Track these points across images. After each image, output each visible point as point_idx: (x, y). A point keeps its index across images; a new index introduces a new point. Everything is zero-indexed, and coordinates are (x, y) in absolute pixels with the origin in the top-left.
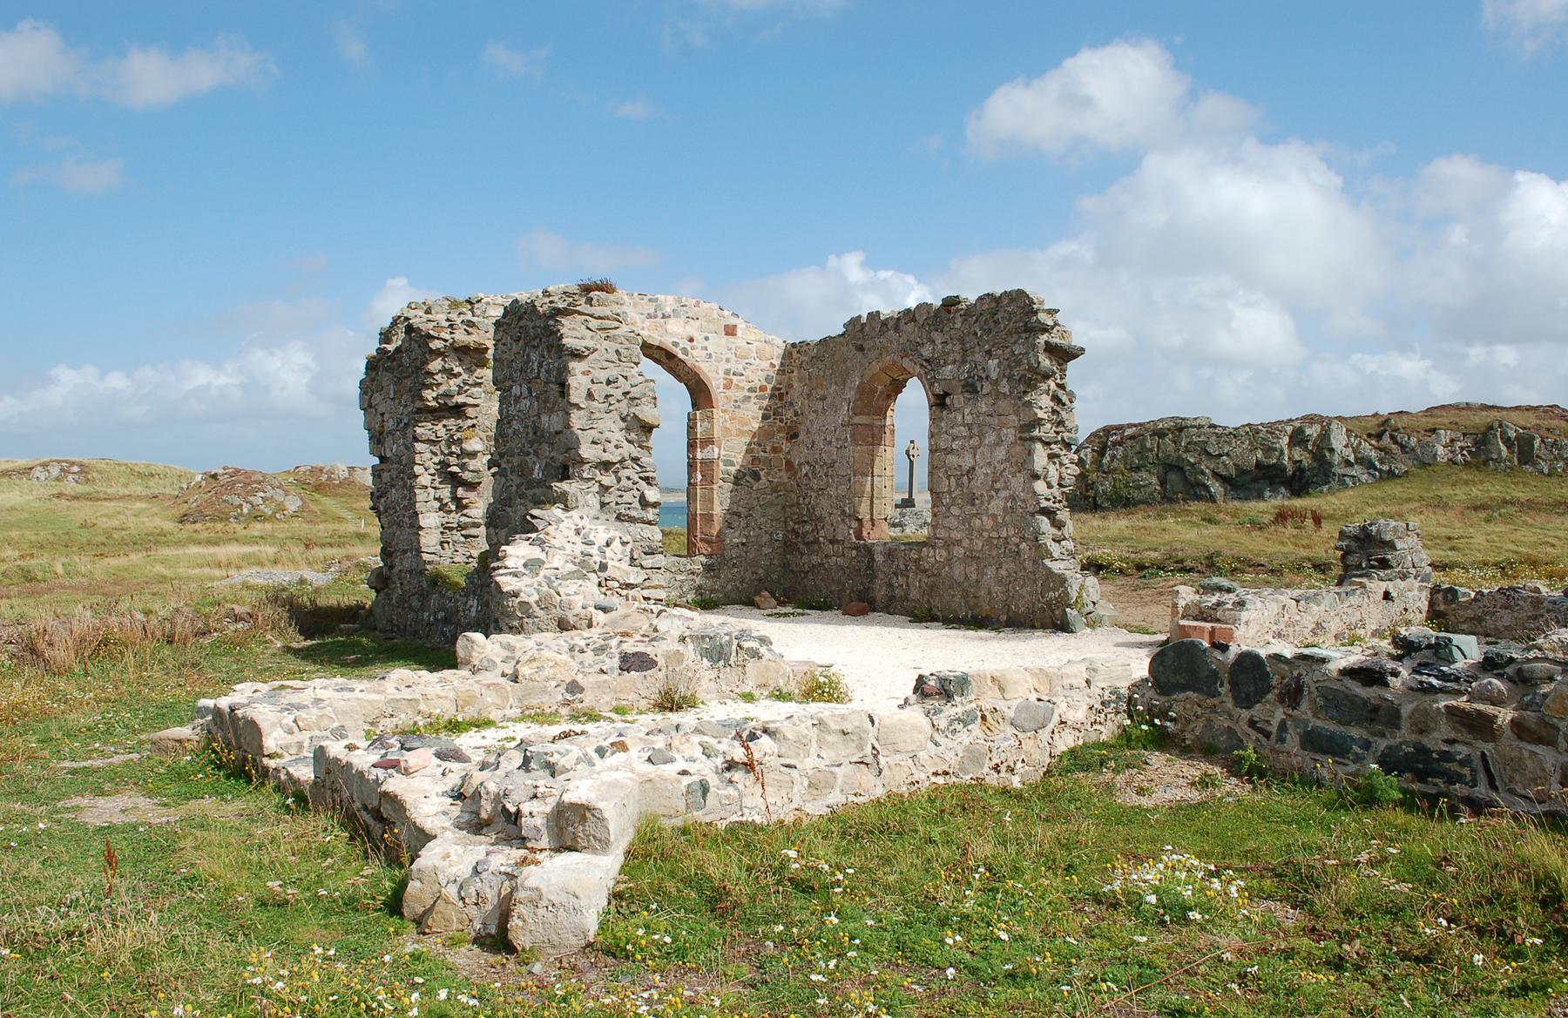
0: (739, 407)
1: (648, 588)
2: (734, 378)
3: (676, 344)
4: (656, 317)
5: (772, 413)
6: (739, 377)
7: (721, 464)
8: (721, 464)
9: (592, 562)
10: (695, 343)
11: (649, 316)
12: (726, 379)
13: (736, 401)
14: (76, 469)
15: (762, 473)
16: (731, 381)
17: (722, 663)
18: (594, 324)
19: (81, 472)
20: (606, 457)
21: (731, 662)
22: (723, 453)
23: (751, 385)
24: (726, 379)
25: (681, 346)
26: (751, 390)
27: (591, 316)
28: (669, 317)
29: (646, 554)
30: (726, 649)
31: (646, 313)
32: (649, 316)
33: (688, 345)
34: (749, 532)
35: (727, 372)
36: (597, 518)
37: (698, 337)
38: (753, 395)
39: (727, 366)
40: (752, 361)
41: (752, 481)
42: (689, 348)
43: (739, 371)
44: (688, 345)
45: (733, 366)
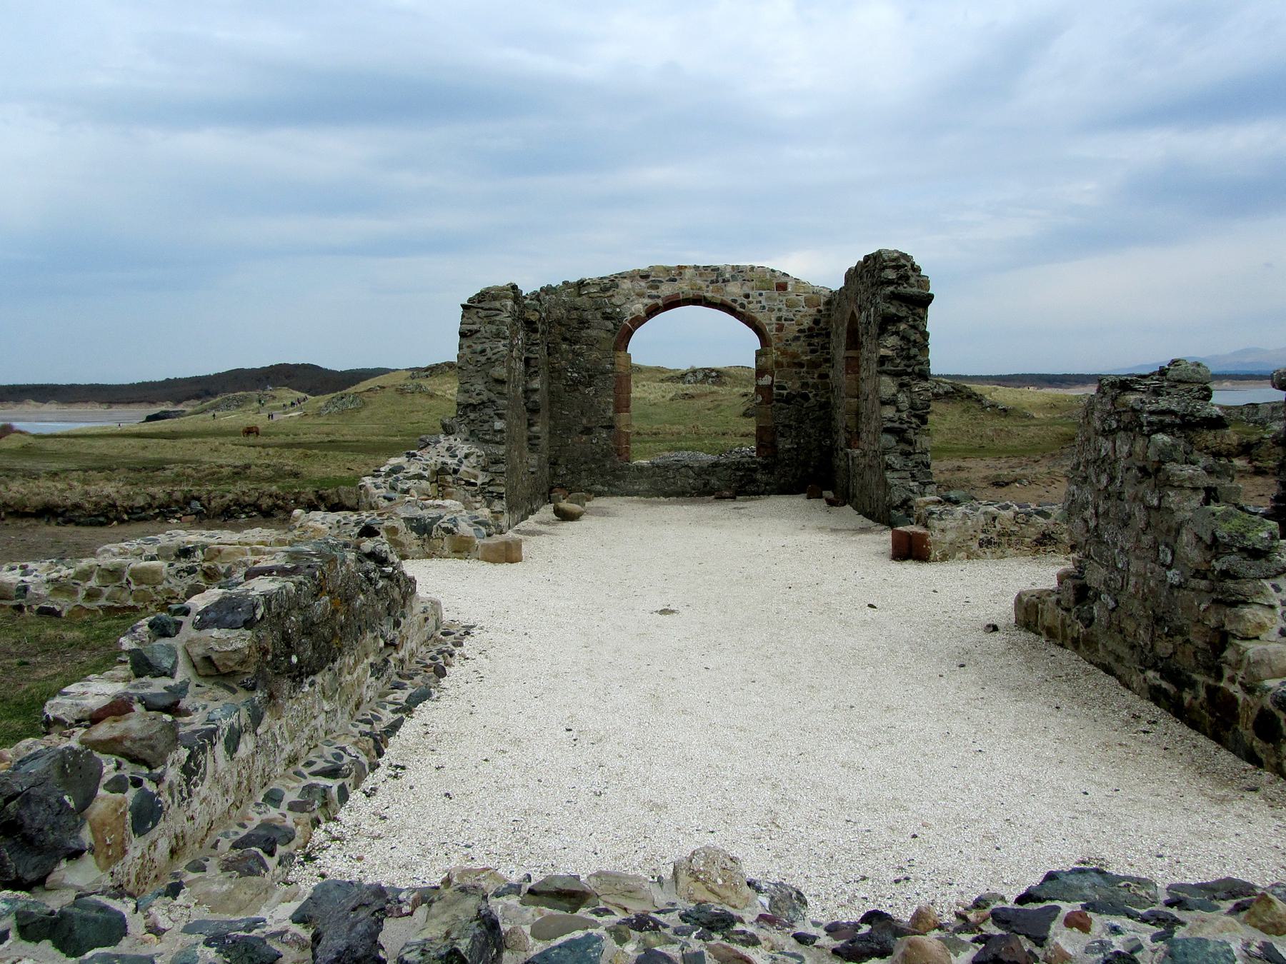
0: (790, 345)
1: (492, 485)
2: (786, 323)
3: (734, 301)
4: (717, 282)
5: (819, 348)
6: (789, 322)
7: (774, 389)
8: (774, 389)
9: (448, 468)
10: (751, 299)
11: (712, 282)
12: (778, 324)
13: (787, 341)
14: (714, 374)
15: (811, 395)
16: (783, 325)
17: (426, 535)
18: (482, 313)
19: (717, 376)
20: (471, 401)
21: (433, 535)
22: (775, 380)
23: (801, 327)
24: (778, 324)
25: (739, 302)
26: (800, 331)
27: (482, 308)
28: (729, 281)
29: (493, 463)
30: (430, 527)
31: (710, 279)
32: (712, 282)
33: (745, 301)
34: (800, 440)
35: (779, 319)
36: (467, 440)
37: (754, 293)
38: (802, 335)
39: (779, 314)
40: (801, 309)
41: (803, 401)
42: (746, 303)
43: (789, 317)
44: (745, 301)
45: (784, 314)
